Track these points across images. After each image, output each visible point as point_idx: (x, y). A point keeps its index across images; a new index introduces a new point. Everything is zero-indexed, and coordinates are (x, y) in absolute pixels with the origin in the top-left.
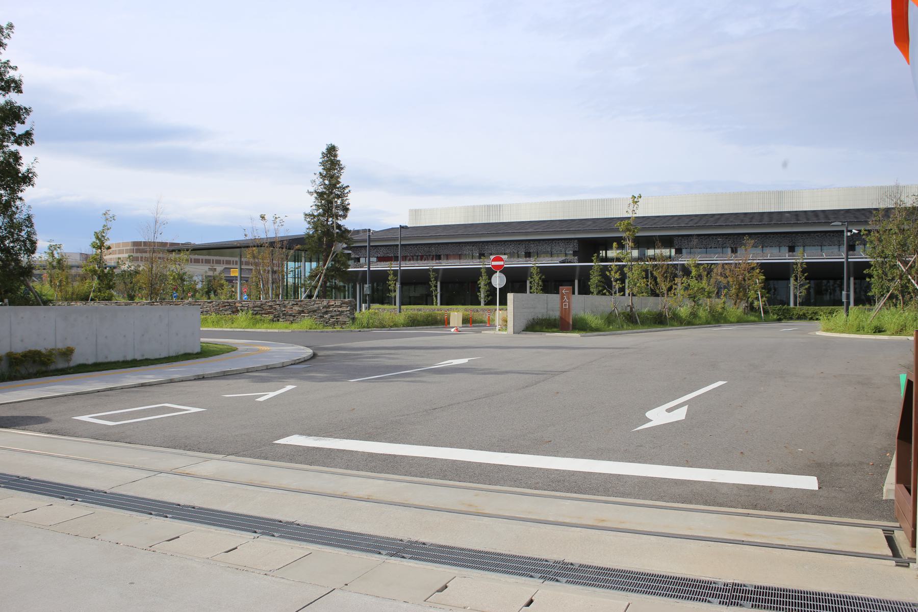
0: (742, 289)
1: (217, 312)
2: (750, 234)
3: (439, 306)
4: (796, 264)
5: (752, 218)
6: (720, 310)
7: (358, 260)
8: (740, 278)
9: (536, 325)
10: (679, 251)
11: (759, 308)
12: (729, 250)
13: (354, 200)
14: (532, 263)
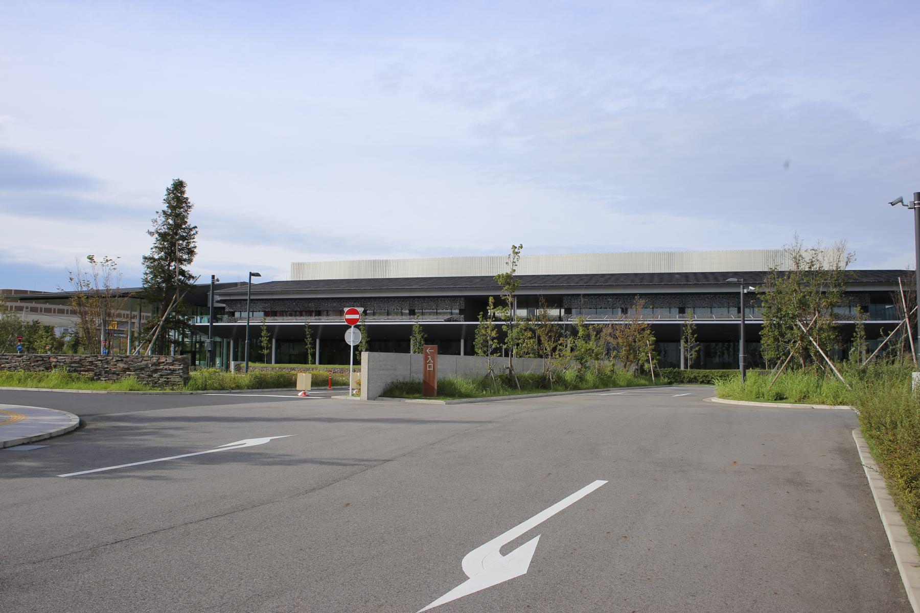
0: (633, 350)
1: (27, 368)
2: (641, 295)
3: (273, 364)
4: (686, 325)
5: (642, 279)
6: (609, 373)
7: (233, 314)
8: (631, 339)
9: (397, 390)
10: (568, 311)
11: (650, 371)
12: (620, 310)
13: (200, 243)
14: (258, 320)
